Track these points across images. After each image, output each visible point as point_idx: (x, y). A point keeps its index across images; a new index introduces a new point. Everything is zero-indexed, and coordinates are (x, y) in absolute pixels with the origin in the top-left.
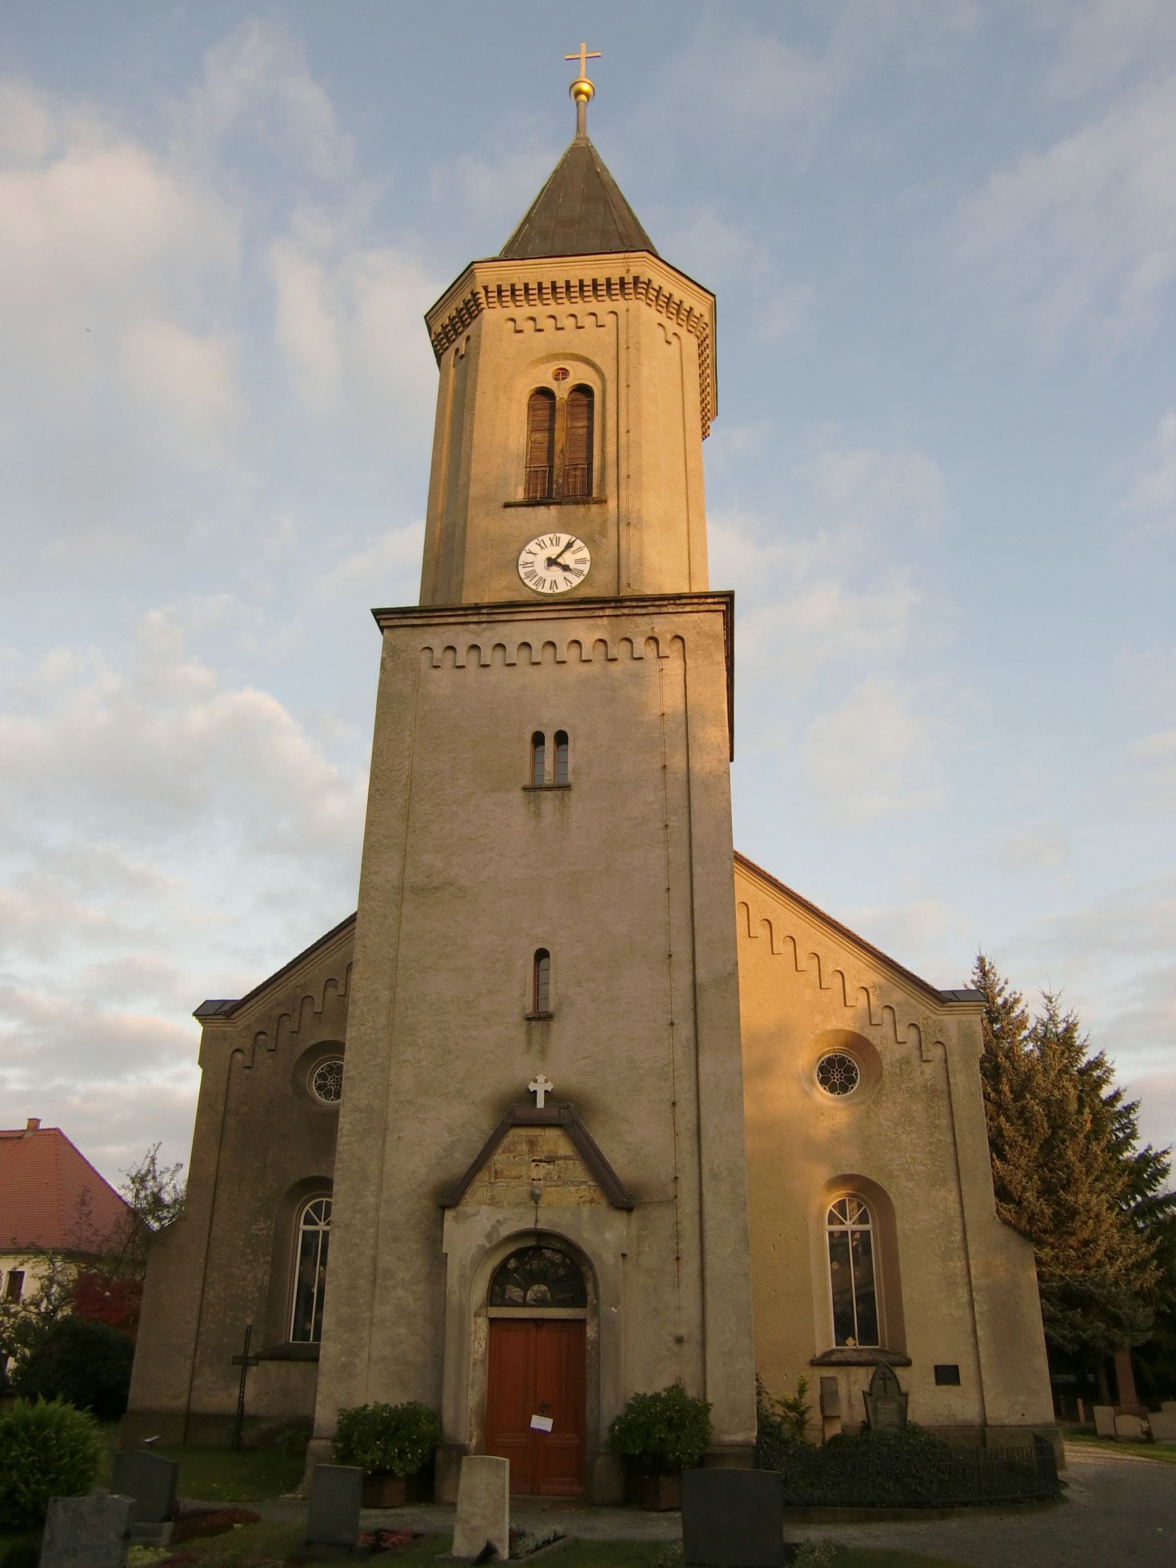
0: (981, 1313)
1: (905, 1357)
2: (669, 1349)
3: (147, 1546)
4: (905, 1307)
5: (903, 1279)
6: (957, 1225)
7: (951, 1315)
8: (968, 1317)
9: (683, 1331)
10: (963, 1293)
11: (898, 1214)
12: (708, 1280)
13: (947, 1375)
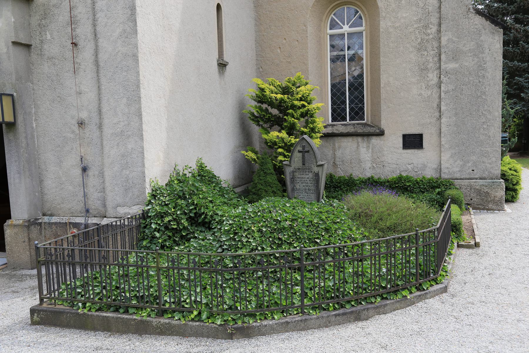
0: (446, 93)
1: (379, 128)
2: (73, 132)
3: (360, 161)
4: (382, 91)
5: (382, 68)
6: (434, 20)
7: (420, 95)
8: (436, 96)
9: (84, 115)
10: (433, 77)
11: (383, 14)
12: (101, 64)
13: (413, 141)
